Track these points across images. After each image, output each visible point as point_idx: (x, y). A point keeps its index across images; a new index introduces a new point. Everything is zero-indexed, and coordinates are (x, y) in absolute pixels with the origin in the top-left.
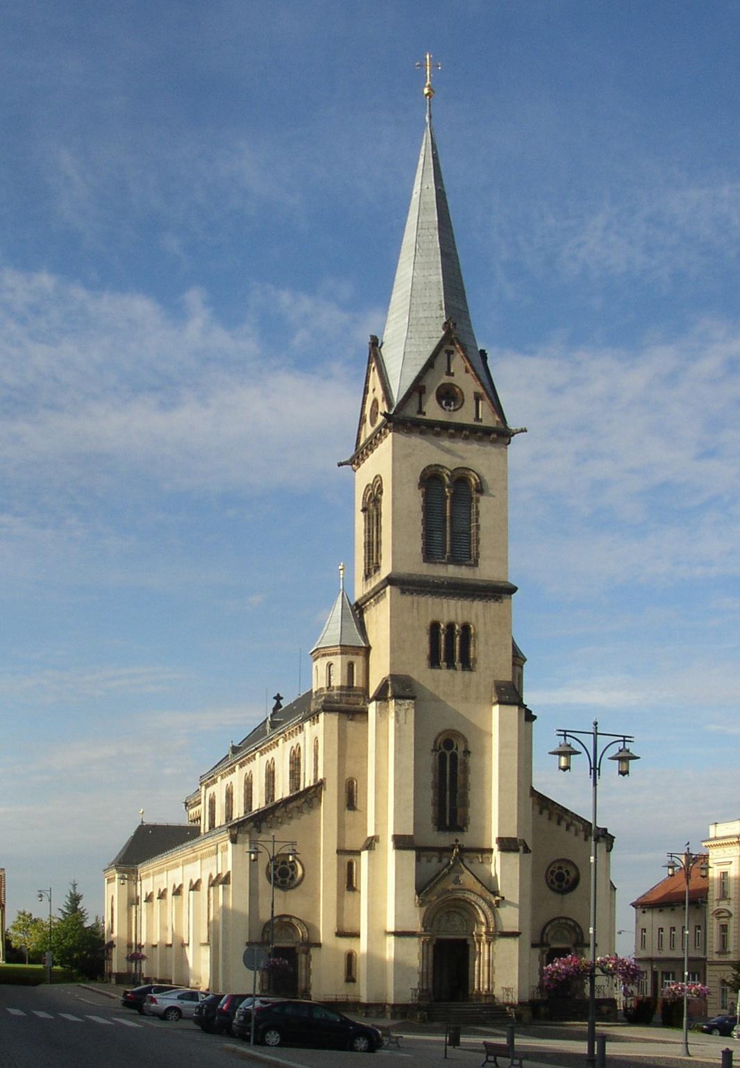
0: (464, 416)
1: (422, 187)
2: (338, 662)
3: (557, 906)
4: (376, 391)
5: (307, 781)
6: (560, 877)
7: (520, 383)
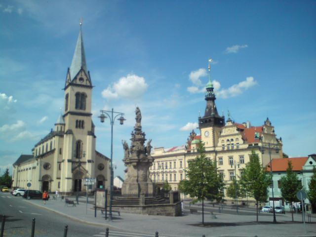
0: (84, 83)
1: (79, 41)
2: (59, 126)
3: (100, 173)
4: (68, 78)
5: (53, 148)
6: (101, 167)
7: (95, 77)
